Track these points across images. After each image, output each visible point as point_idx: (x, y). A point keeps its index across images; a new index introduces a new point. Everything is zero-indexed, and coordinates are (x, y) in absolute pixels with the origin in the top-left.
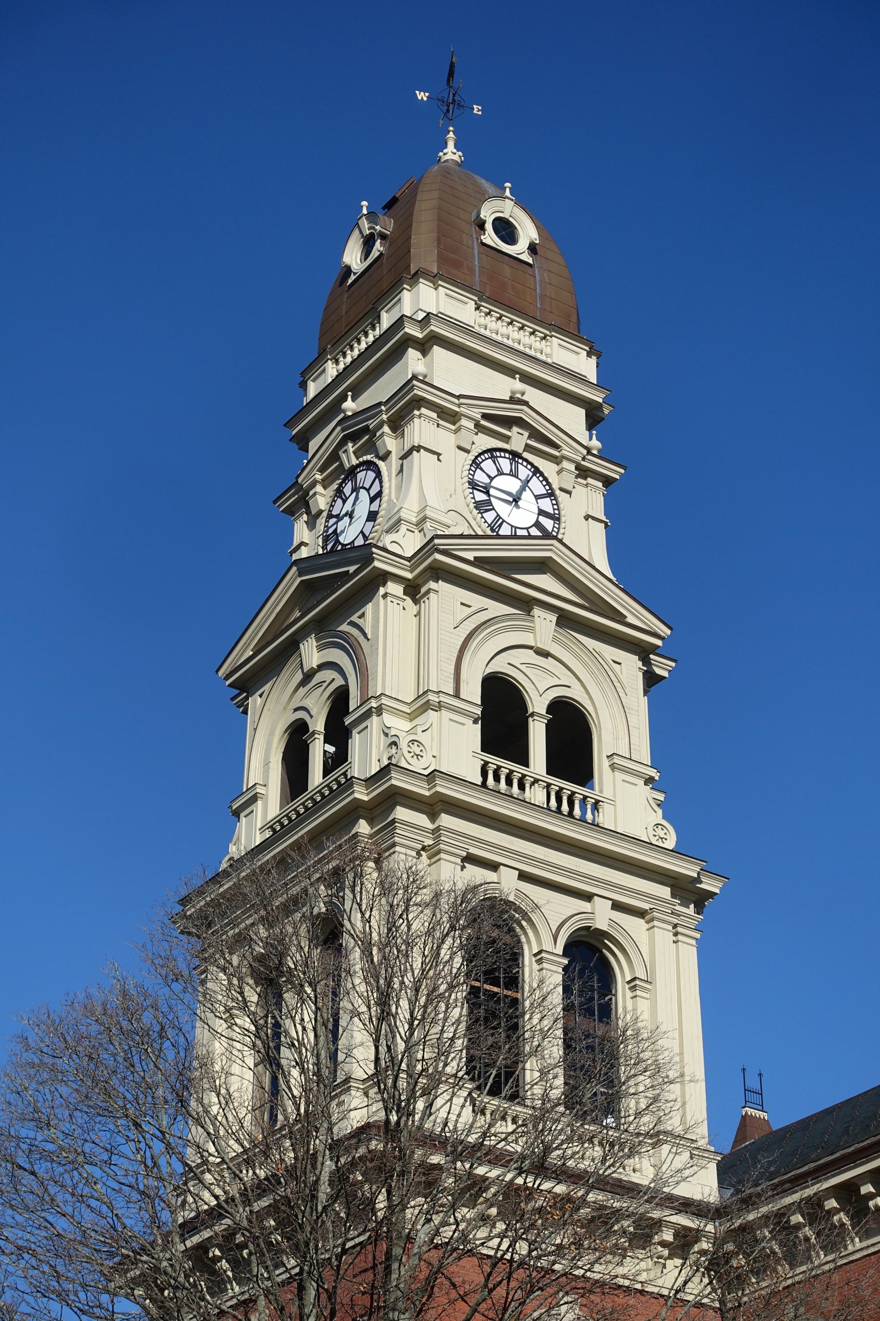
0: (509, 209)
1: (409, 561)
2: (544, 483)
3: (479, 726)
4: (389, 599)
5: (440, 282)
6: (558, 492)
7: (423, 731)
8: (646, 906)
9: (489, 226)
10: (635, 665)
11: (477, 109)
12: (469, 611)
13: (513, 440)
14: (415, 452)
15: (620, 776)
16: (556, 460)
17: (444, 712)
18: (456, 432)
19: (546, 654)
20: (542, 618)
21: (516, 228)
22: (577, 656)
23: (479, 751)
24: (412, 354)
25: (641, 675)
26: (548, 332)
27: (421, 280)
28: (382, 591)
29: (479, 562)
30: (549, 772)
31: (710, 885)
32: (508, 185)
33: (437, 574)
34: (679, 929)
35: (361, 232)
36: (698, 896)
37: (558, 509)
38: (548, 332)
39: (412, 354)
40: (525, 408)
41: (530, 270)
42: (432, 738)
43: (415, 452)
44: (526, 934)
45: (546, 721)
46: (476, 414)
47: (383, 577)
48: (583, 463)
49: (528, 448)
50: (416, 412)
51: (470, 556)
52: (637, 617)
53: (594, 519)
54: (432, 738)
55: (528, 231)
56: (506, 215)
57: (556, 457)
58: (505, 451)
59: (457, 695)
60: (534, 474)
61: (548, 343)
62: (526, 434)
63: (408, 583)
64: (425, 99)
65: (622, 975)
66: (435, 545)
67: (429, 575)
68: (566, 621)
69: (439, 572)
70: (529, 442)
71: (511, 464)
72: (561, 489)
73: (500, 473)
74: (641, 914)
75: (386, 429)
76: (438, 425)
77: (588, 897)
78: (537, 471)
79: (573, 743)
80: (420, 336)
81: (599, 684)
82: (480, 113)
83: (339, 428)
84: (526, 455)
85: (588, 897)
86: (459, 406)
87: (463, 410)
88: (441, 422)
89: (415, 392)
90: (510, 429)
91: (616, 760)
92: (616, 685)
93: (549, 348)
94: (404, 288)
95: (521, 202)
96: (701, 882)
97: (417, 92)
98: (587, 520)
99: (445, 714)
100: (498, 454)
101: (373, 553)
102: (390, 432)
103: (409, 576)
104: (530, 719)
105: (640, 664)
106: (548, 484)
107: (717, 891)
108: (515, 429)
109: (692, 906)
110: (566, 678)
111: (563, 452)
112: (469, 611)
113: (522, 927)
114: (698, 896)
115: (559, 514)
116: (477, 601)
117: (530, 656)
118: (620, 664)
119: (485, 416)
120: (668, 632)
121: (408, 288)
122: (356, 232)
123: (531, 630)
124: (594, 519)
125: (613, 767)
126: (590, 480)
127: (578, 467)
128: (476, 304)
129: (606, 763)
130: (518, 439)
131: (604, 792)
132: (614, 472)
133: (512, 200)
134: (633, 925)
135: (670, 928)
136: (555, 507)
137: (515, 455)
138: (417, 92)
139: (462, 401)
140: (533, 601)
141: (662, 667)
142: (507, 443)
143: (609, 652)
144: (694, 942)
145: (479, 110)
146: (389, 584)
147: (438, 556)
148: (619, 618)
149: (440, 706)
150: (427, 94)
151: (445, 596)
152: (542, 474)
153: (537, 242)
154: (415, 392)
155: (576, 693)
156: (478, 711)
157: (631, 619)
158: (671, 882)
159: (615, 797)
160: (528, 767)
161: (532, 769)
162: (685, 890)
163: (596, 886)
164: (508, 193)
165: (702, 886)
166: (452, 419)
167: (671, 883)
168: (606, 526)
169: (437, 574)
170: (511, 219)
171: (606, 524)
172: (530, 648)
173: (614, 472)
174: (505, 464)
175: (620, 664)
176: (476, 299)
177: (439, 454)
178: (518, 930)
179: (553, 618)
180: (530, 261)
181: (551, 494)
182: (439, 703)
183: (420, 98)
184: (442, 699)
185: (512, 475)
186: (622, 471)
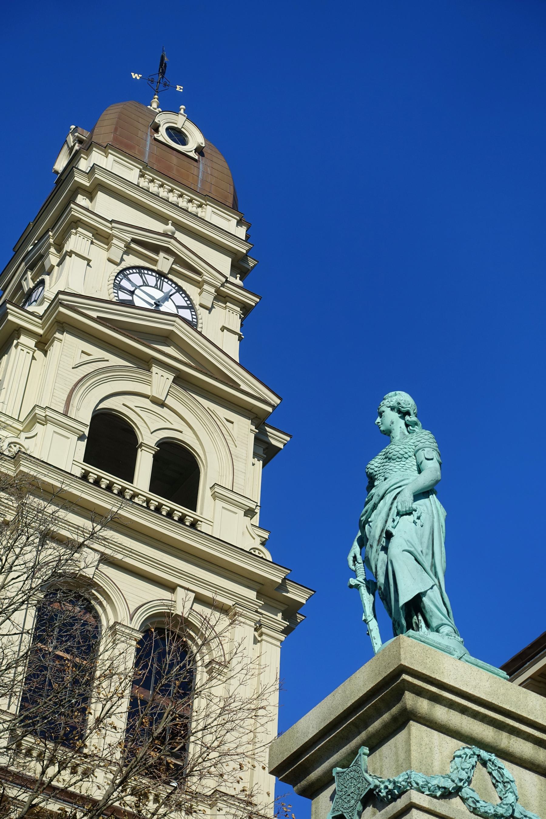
0: (180, 121)
1: (41, 319)
2: (183, 295)
3: (83, 445)
4: (20, 347)
5: (110, 151)
6: (197, 307)
7: (26, 438)
8: (231, 603)
9: (162, 130)
10: (247, 427)
11: (179, 88)
12: (86, 358)
13: (159, 263)
14: (67, 257)
15: (219, 504)
16: (198, 284)
17: (49, 426)
18: (108, 250)
19: (162, 404)
20: (160, 375)
21: (186, 136)
22: (191, 410)
23: (81, 461)
24: (81, 200)
25: (252, 436)
26: (204, 202)
27: (94, 149)
28: (15, 342)
29: (100, 320)
30: (152, 489)
31: (298, 595)
32: (183, 107)
33: (63, 327)
34: (264, 630)
35: (68, 146)
36: (287, 607)
37: (197, 319)
38: (204, 202)
39: (81, 200)
40: (172, 241)
41: (195, 164)
42: (36, 445)
43: (67, 257)
44: (104, 610)
45: (154, 453)
46: (128, 237)
47: (18, 331)
48: (222, 288)
49: (172, 271)
50: (74, 231)
51: (94, 315)
52: (250, 387)
53: (229, 330)
54: (36, 445)
55: (196, 137)
56: (179, 126)
57: (198, 282)
58: (153, 271)
59: (65, 415)
60: (177, 291)
61: (204, 210)
62: (172, 260)
63: (40, 338)
64: (138, 78)
65: (201, 660)
66: (59, 299)
67: (56, 328)
68: (181, 380)
69: (64, 325)
70: (174, 266)
71: (157, 281)
72: (201, 305)
73: (146, 284)
74: (224, 610)
75: (52, 250)
76: (92, 243)
77: (171, 588)
78: (180, 289)
79: (178, 473)
80: (88, 185)
81: (210, 433)
82: (181, 91)
83: (23, 264)
84: (170, 276)
85: (171, 588)
86: (111, 229)
87: (114, 232)
88: (94, 241)
89: (73, 213)
90: (157, 253)
91: (217, 489)
92: (227, 439)
93: (204, 213)
94: (82, 157)
95: (190, 118)
96: (288, 592)
97: (133, 74)
98: (223, 331)
99: (50, 427)
100: (146, 272)
101: (8, 308)
102: (55, 252)
103: (41, 332)
104: (139, 450)
105: (253, 428)
106: (190, 299)
107: (304, 601)
108: (162, 255)
109: (280, 615)
110: (178, 424)
111: (204, 277)
112: (86, 358)
113: (96, 599)
114: (287, 607)
115: (197, 322)
116: (97, 352)
117: (147, 403)
118: (232, 423)
119: (134, 241)
120: (278, 401)
121: (86, 157)
122: (66, 147)
123: (149, 383)
124: (229, 330)
125: (215, 496)
126: (228, 304)
127: (218, 290)
128: (140, 171)
129: (209, 493)
130: (164, 263)
131: (204, 514)
132: (251, 300)
133: (184, 116)
134: (220, 622)
135: (253, 624)
136: (195, 317)
137: (161, 275)
138: (133, 74)
139: (114, 225)
140: (152, 360)
141: (278, 439)
142: (155, 266)
143: (223, 413)
144: (279, 644)
145: (181, 89)
146: (22, 337)
147: (61, 309)
148: (236, 386)
149: (45, 421)
150: (140, 76)
151: (67, 346)
152: (184, 292)
153: (204, 145)
154: (73, 213)
155: (187, 437)
156: (86, 432)
157: (243, 387)
158: (258, 587)
159: (213, 519)
160: (132, 483)
161: (135, 485)
162: (270, 595)
163: (180, 578)
164: (182, 111)
165: (288, 595)
166: (106, 240)
167: (258, 588)
168: (240, 339)
169: (63, 327)
170: (182, 129)
171: (240, 336)
172: (147, 397)
173: (251, 300)
174: (151, 280)
175: (232, 423)
176: (141, 167)
177: (89, 261)
178: (98, 608)
179: (171, 377)
180: (197, 157)
181: (191, 307)
182: (45, 417)
183: (134, 77)
184: (47, 413)
185: (157, 288)
186: (258, 300)
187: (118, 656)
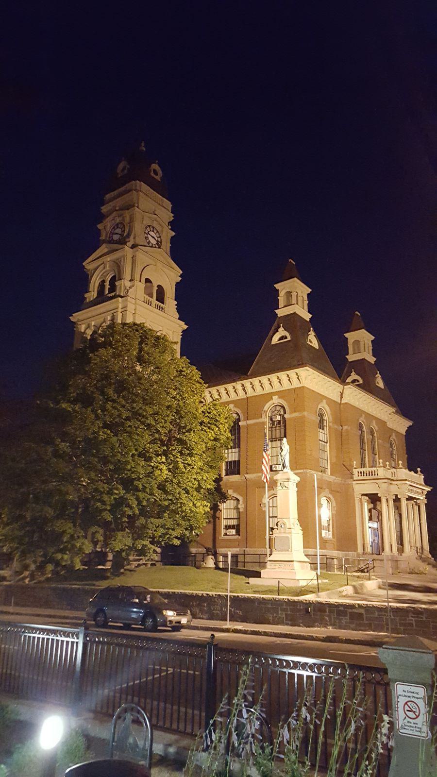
73: (151, 231)
187: (393, 475)
